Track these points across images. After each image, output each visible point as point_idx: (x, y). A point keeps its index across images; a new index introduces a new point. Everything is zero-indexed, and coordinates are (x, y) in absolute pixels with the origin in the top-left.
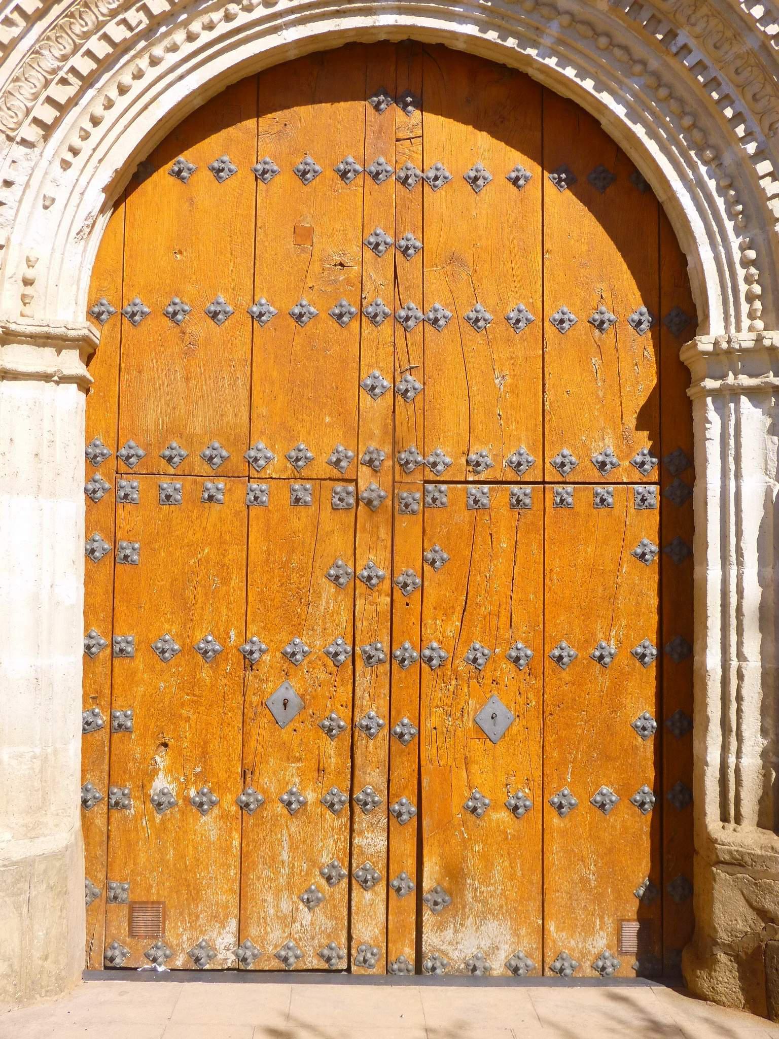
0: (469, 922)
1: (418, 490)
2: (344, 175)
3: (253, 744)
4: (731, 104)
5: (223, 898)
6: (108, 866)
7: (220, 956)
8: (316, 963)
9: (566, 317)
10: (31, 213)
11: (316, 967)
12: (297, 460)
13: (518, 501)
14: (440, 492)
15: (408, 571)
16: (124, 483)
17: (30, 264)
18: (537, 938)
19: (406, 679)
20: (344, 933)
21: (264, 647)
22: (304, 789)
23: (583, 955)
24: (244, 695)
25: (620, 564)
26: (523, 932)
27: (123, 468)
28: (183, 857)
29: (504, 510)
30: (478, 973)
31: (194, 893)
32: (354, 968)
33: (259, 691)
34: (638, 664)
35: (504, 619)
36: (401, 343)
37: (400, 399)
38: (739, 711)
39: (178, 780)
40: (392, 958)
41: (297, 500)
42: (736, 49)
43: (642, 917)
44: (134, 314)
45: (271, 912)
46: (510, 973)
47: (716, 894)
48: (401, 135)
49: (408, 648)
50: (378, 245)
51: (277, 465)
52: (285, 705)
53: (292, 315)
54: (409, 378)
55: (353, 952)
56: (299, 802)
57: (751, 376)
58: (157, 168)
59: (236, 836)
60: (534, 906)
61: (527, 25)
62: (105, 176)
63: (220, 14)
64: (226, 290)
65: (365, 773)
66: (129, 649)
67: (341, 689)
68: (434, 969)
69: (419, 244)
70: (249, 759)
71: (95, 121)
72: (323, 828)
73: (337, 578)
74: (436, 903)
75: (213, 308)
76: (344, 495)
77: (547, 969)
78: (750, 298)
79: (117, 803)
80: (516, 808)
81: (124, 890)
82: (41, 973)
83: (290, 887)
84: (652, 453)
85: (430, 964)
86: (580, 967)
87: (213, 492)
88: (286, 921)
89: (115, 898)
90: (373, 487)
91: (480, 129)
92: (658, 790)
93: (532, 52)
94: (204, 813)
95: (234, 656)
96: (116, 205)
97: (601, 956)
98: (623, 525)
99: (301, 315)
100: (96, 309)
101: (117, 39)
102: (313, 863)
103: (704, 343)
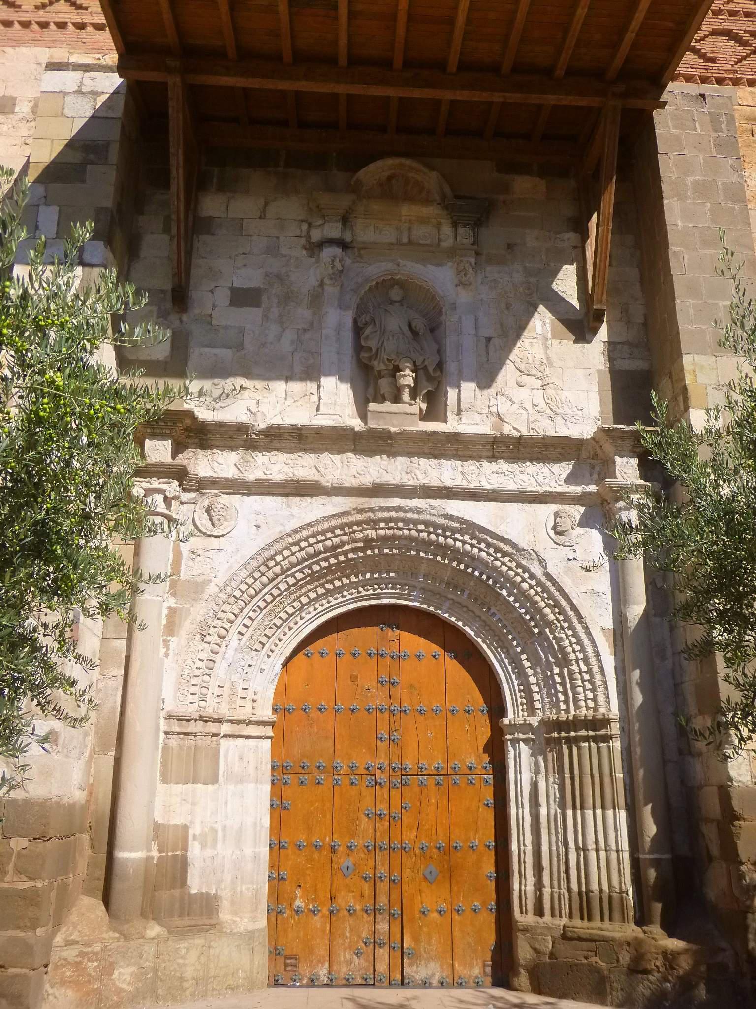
0: (423, 962)
2: (370, 655)
5: (322, 953)
15: (396, 811)
17: (255, 693)
18: (450, 969)
20: (372, 967)
23: (470, 977)
25: (479, 808)
27: (285, 771)
29: (433, 786)
32: (376, 984)
33: (337, 863)
34: (487, 849)
35: (434, 832)
36: (392, 720)
37: (392, 742)
38: (525, 867)
40: (392, 979)
45: (342, 959)
49: (396, 843)
51: (344, 770)
53: (350, 709)
55: (376, 976)
57: (523, 734)
62: (283, 659)
63: (326, 600)
68: (409, 983)
70: (333, 891)
71: (280, 640)
73: (368, 815)
74: (409, 954)
78: (522, 704)
80: (441, 912)
83: (350, 948)
84: (489, 763)
85: (407, 981)
86: (469, 982)
88: (349, 963)
89: (279, 953)
92: (497, 904)
93: (439, 612)
94: (315, 915)
95: (327, 848)
97: (477, 977)
99: (354, 710)
101: (290, 612)
102: (359, 936)
103: (506, 721)
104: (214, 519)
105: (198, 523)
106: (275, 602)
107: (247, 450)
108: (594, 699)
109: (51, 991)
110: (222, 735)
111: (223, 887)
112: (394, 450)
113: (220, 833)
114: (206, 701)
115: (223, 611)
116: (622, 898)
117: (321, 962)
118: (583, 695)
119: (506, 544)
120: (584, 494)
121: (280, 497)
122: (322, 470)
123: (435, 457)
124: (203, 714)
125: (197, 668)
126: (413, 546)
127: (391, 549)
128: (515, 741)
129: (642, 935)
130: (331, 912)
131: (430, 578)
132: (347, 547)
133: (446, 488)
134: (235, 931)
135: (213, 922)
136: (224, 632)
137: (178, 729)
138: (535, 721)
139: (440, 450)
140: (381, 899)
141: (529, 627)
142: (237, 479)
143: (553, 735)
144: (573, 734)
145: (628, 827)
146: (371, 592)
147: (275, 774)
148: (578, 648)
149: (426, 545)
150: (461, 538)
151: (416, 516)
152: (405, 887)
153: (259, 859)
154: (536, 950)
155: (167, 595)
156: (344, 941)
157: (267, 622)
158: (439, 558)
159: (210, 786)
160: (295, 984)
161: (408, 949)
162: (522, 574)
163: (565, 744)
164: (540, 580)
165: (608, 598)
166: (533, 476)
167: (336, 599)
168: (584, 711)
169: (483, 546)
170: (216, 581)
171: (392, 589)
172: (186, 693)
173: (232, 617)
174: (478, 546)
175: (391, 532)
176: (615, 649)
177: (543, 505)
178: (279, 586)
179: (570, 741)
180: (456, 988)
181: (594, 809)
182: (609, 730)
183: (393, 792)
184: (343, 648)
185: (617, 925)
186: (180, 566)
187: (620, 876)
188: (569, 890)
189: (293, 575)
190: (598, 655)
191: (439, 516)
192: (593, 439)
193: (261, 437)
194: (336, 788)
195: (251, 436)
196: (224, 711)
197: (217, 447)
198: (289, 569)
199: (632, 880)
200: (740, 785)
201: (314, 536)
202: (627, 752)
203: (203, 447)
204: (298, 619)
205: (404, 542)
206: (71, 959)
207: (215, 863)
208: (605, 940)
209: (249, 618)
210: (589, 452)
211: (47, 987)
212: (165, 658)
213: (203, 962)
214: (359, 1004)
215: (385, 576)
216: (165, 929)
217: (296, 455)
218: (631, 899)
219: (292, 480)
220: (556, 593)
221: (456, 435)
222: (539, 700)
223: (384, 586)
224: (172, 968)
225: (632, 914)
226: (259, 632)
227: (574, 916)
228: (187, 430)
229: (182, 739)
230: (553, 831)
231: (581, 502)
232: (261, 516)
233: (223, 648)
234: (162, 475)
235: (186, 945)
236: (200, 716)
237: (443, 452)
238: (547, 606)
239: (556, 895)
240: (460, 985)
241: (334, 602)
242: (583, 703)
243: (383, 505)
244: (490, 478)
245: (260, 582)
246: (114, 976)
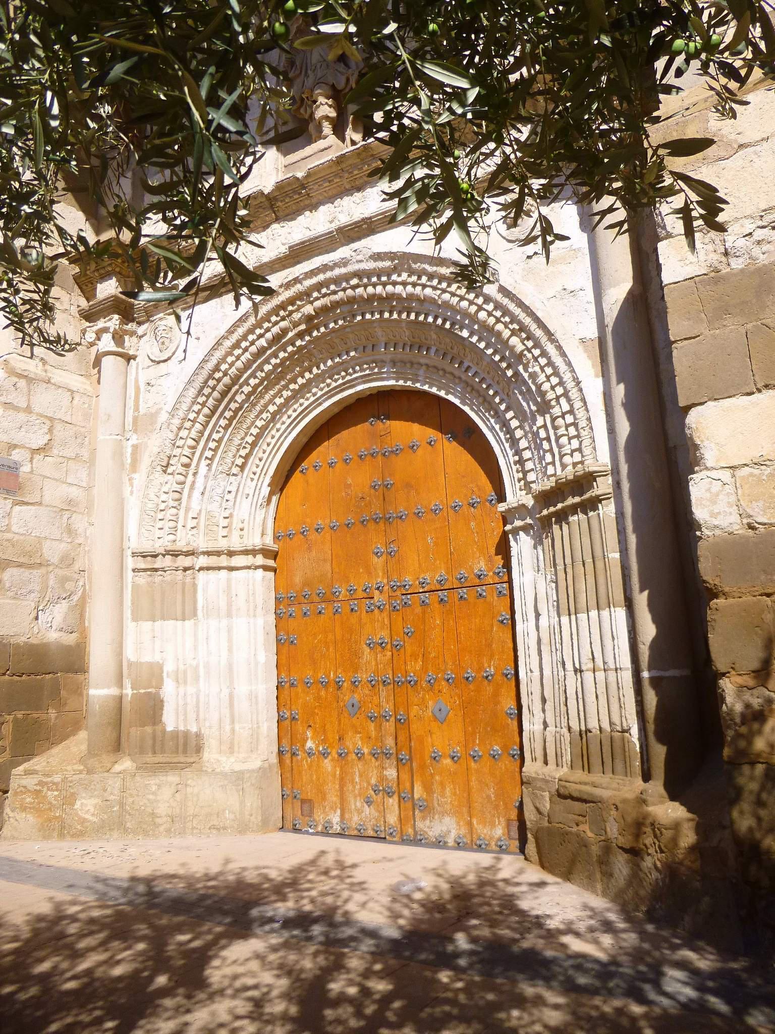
0: (436, 817)
26: (461, 823)
29: (437, 605)
31: (324, 798)
45: (353, 807)
60: (465, 810)
61: (412, 374)
83: (360, 795)
88: (360, 811)
94: (326, 758)
96: (282, 490)
97: (500, 839)
102: (369, 783)
109: (11, 815)
115: (181, 438)
116: (623, 739)
125: (163, 502)
132: (290, 334)
134: (218, 770)
137: (143, 566)
150: (399, 279)
151: (343, 270)
152: (414, 727)
156: (354, 787)
157: (237, 441)
161: (419, 799)
185: (619, 778)
194: (337, 616)
196: (202, 544)
200: (718, 532)
205: (346, 308)
206: (31, 787)
211: (7, 810)
213: (178, 800)
219: (215, 276)
224: (141, 804)
233: (190, 478)
234: (105, 313)
235: (157, 781)
236: (165, 551)
241: (306, 403)
243: (307, 270)
246: (76, 807)
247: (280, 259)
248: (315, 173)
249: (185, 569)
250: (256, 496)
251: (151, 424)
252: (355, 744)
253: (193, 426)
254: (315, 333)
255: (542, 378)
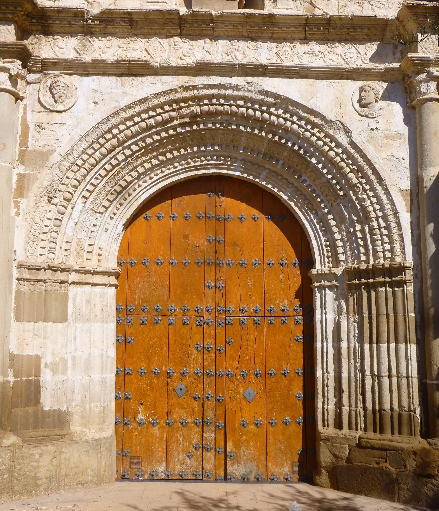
0: (242, 463)
1: (224, 319)
2: (199, 218)
3: (170, 403)
4: (319, 197)
6: (123, 445)
7: (160, 475)
8: (192, 477)
9: (271, 262)
10: (101, 234)
11: (191, 478)
12: (185, 310)
13: (256, 323)
14: (231, 320)
15: (221, 346)
16: (129, 318)
17: (101, 249)
18: (265, 468)
19: (220, 381)
20: (201, 467)
21: (174, 371)
22: (187, 418)
24: (167, 387)
27: (128, 313)
28: (148, 441)
29: (252, 325)
30: (245, 480)
31: (151, 454)
32: (204, 479)
34: (297, 376)
35: (252, 361)
38: (327, 390)
39: (146, 415)
40: (217, 475)
41: (185, 323)
42: (320, 181)
43: (300, 461)
44: (132, 263)
45: (177, 460)
46: (256, 480)
47: (321, 450)
48: (217, 205)
49: (221, 371)
50: (210, 240)
52: (181, 390)
53: (183, 263)
54: (221, 283)
55: (204, 473)
56: (186, 422)
57: (328, 282)
58: (139, 216)
59: (165, 434)
62: (124, 221)
63: (160, 171)
64: (161, 255)
65: (207, 413)
66: (130, 372)
67: (199, 385)
68: (231, 479)
69: (223, 239)
70: (169, 409)
72: (193, 431)
73: (198, 348)
74: (231, 456)
75: (157, 261)
76: (200, 321)
77: (268, 479)
78: (328, 257)
79: (126, 423)
80: (257, 424)
81: (128, 452)
82: (104, 476)
83: (183, 451)
84: (300, 306)
85: (229, 477)
86: (279, 478)
87: (157, 320)
88: (182, 462)
89: (125, 455)
90: (209, 318)
91: (243, 202)
92: (304, 418)
93: (258, 180)
94: (154, 426)
97: (286, 474)
98: (291, 330)
99: (185, 263)
100: (120, 262)
101: (129, 181)
102: (191, 443)
103: (314, 272)
104: (56, 96)
105: (42, 100)
106: (113, 171)
107: (85, 36)
108: (392, 251)
110: (69, 283)
111: (74, 404)
112: (215, 33)
113: (70, 362)
114: (54, 254)
115: (67, 178)
116: (410, 415)
117: (159, 462)
118: (382, 247)
119: (315, 117)
120: (387, 70)
121: (114, 77)
122: (152, 52)
123: (253, 40)
124: (51, 264)
125: (46, 226)
126: (234, 121)
127: (214, 124)
128: (322, 288)
129: (427, 447)
130: (168, 424)
131: (249, 149)
132: (175, 122)
133: (262, 66)
134: (84, 439)
135: (64, 432)
136: (68, 196)
137: (28, 277)
138: (338, 271)
139: (257, 33)
140: (208, 415)
141: (335, 191)
142: (75, 60)
143: (354, 282)
144: (371, 280)
145: (418, 357)
146: (199, 163)
147: (120, 316)
148: (377, 207)
149: (246, 118)
150: (275, 112)
151: (235, 93)
153: (106, 383)
154: (335, 456)
155: (17, 163)
158: (256, 131)
159: (60, 324)
160: (138, 479)
162: (329, 144)
163: (364, 289)
164: (346, 148)
165: (406, 163)
166: (341, 56)
167: (169, 169)
168: (382, 261)
169: (295, 119)
170: (59, 151)
171: (216, 160)
172: (35, 246)
173: (76, 183)
174: (291, 119)
175: (214, 107)
176: (411, 207)
177: (349, 81)
178: (117, 156)
179: (369, 287)
180: (270, 483)
181: (388, 342)
182: (404, 276)
183: (219, 330)
184: (177, 213)
185: (405, 438)
186: (28, 138)
187: (409, 397)
188: (365, 408)
189: (129, 147)
190: (395, 213)
191: (256, 93)
192: (397, 18)
193: (96, 22)
195: (87, 21)
196: (72, 262)
197: (58, 33)
198: (125, 142)
199: (420, 401)
201: (146, 111)
202: (419, 295)
203: (46, 33)
204: (136, 186)
205: (225, 118)
207: (66, 386)
208: (394, 449)
209: (92, 184)
210: (393, 32)
212: (16, 217)
213: (55, 464)
214: (185, 499)
215: (210, 148)
216: (20, 439)
217: (128, 40)
218: (419, 417)
219: (124, 61)
220: (360, 160)
221: (272, 16)
222: (342, 253)
223: (209, 158)
225: (418, 428)
226: (101, 197)
227: (368, 429)
228: (29, 16)
229: (33, 285)
230: (352, 361)
231: (384, 78)
232: (98, 94)
233: (69, 210)
234: (6, 55)
235: (40, 451)
236: (49, 266)
237: (260, 35)
238: (352, 171)
239: (353, 413)
240: (273, 481)
241: (167, 172)
242: (381, 254)
244: (302, 58)
245: (100, 153)
247: (186, 67)
248: (226, 17)
249: (62, 282)
250: (113, 231)
251: (42, 161)
252: (180, 416)
253: (79, 170)
254: (195, 127)
255: (368, 203)
